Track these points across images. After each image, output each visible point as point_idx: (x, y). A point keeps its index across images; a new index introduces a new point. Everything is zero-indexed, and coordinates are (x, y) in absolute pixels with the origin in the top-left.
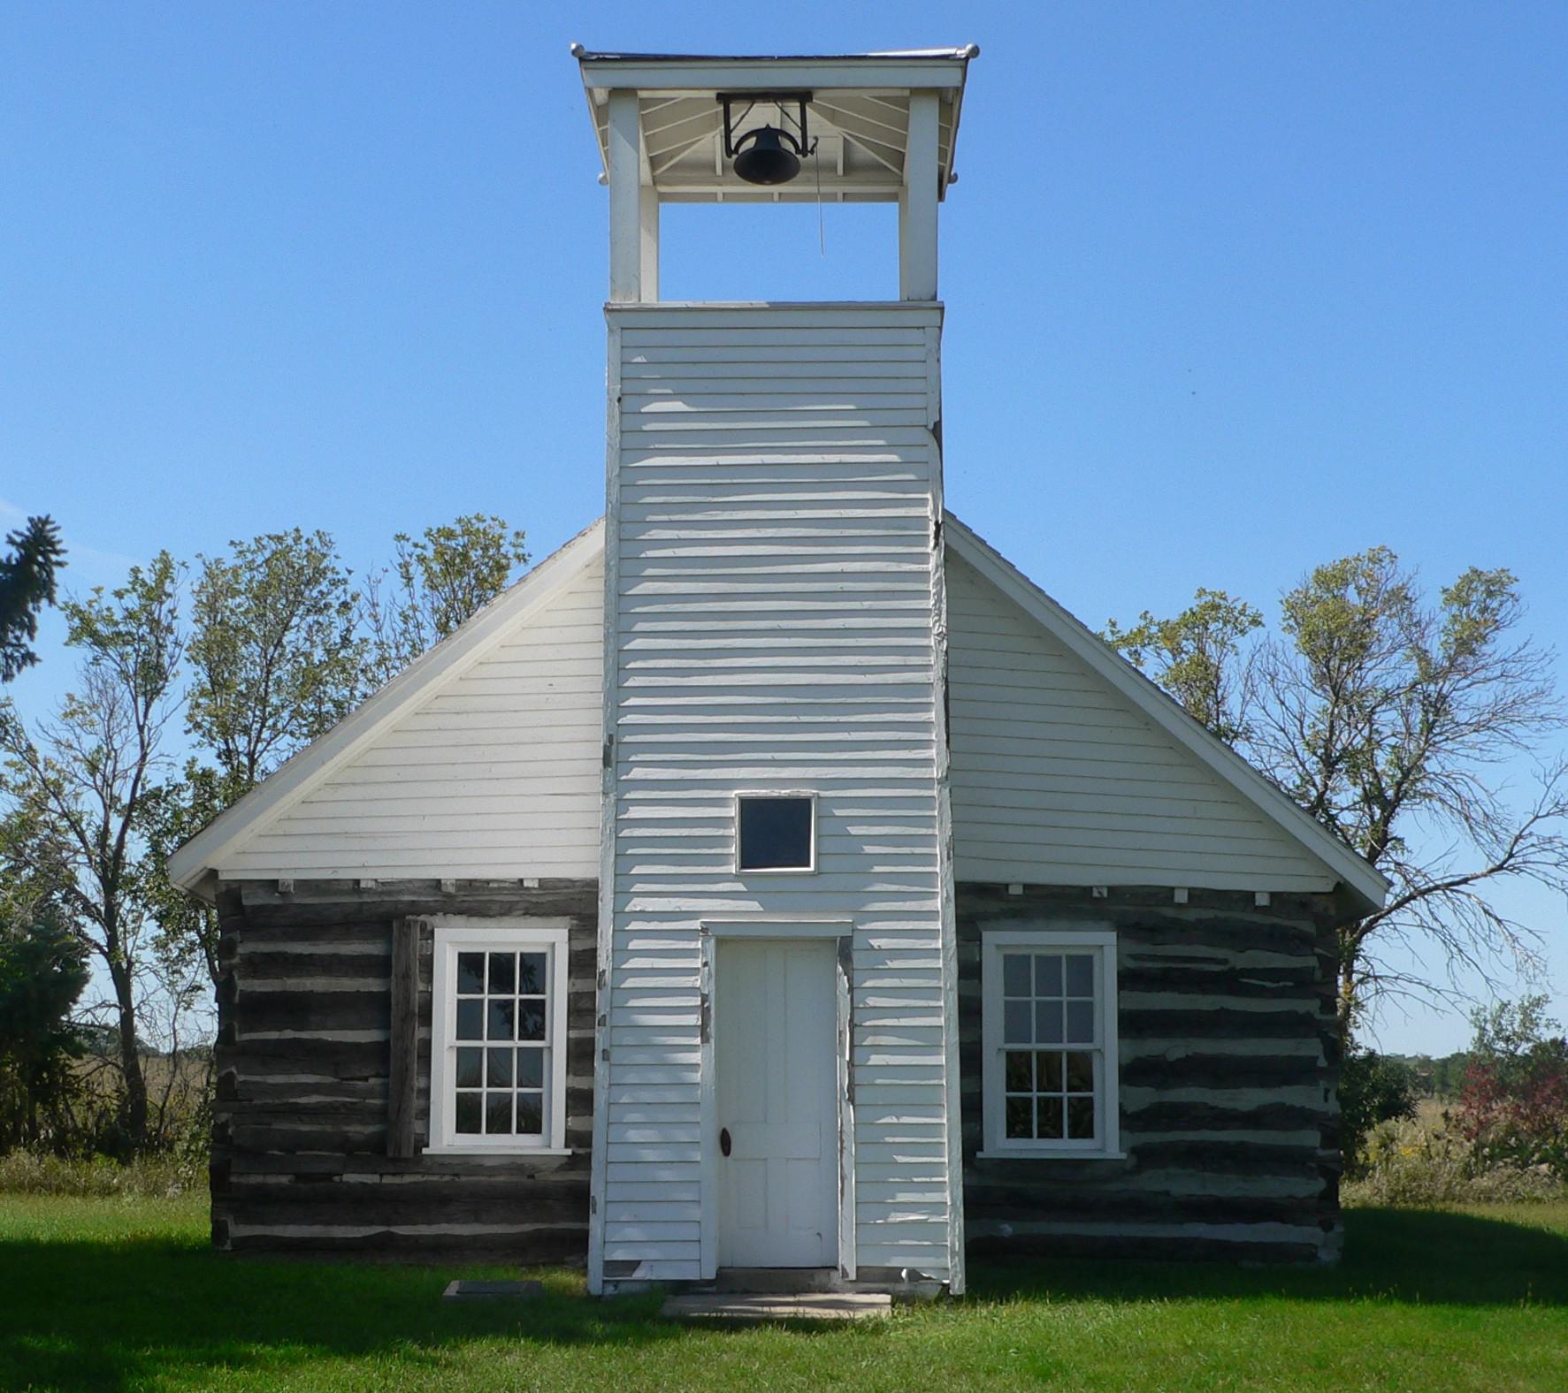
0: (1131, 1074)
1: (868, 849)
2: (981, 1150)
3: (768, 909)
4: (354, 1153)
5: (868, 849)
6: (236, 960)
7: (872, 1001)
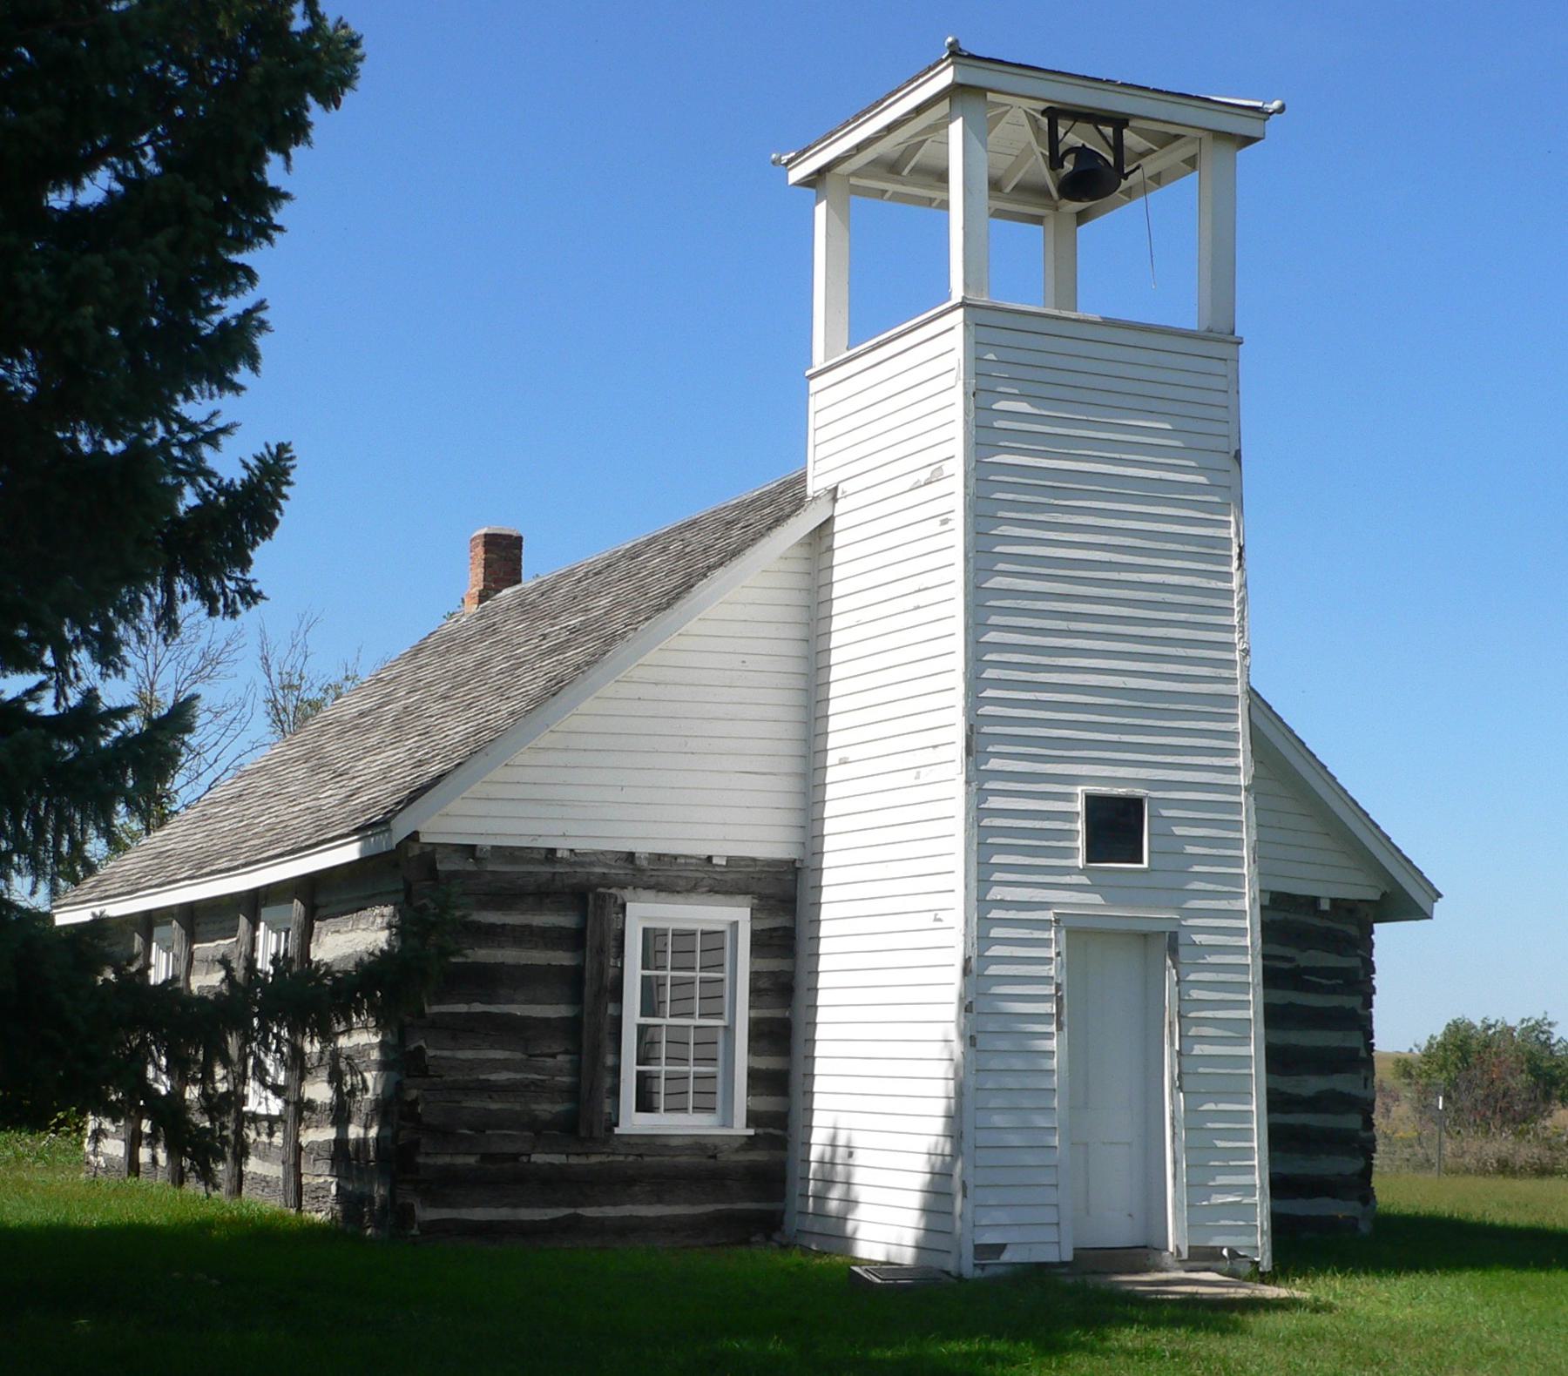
1: (1190, 849)
3: (1111, 902)
4: (540, 1131)
5: (1190, 849)
7: (1196, 994)
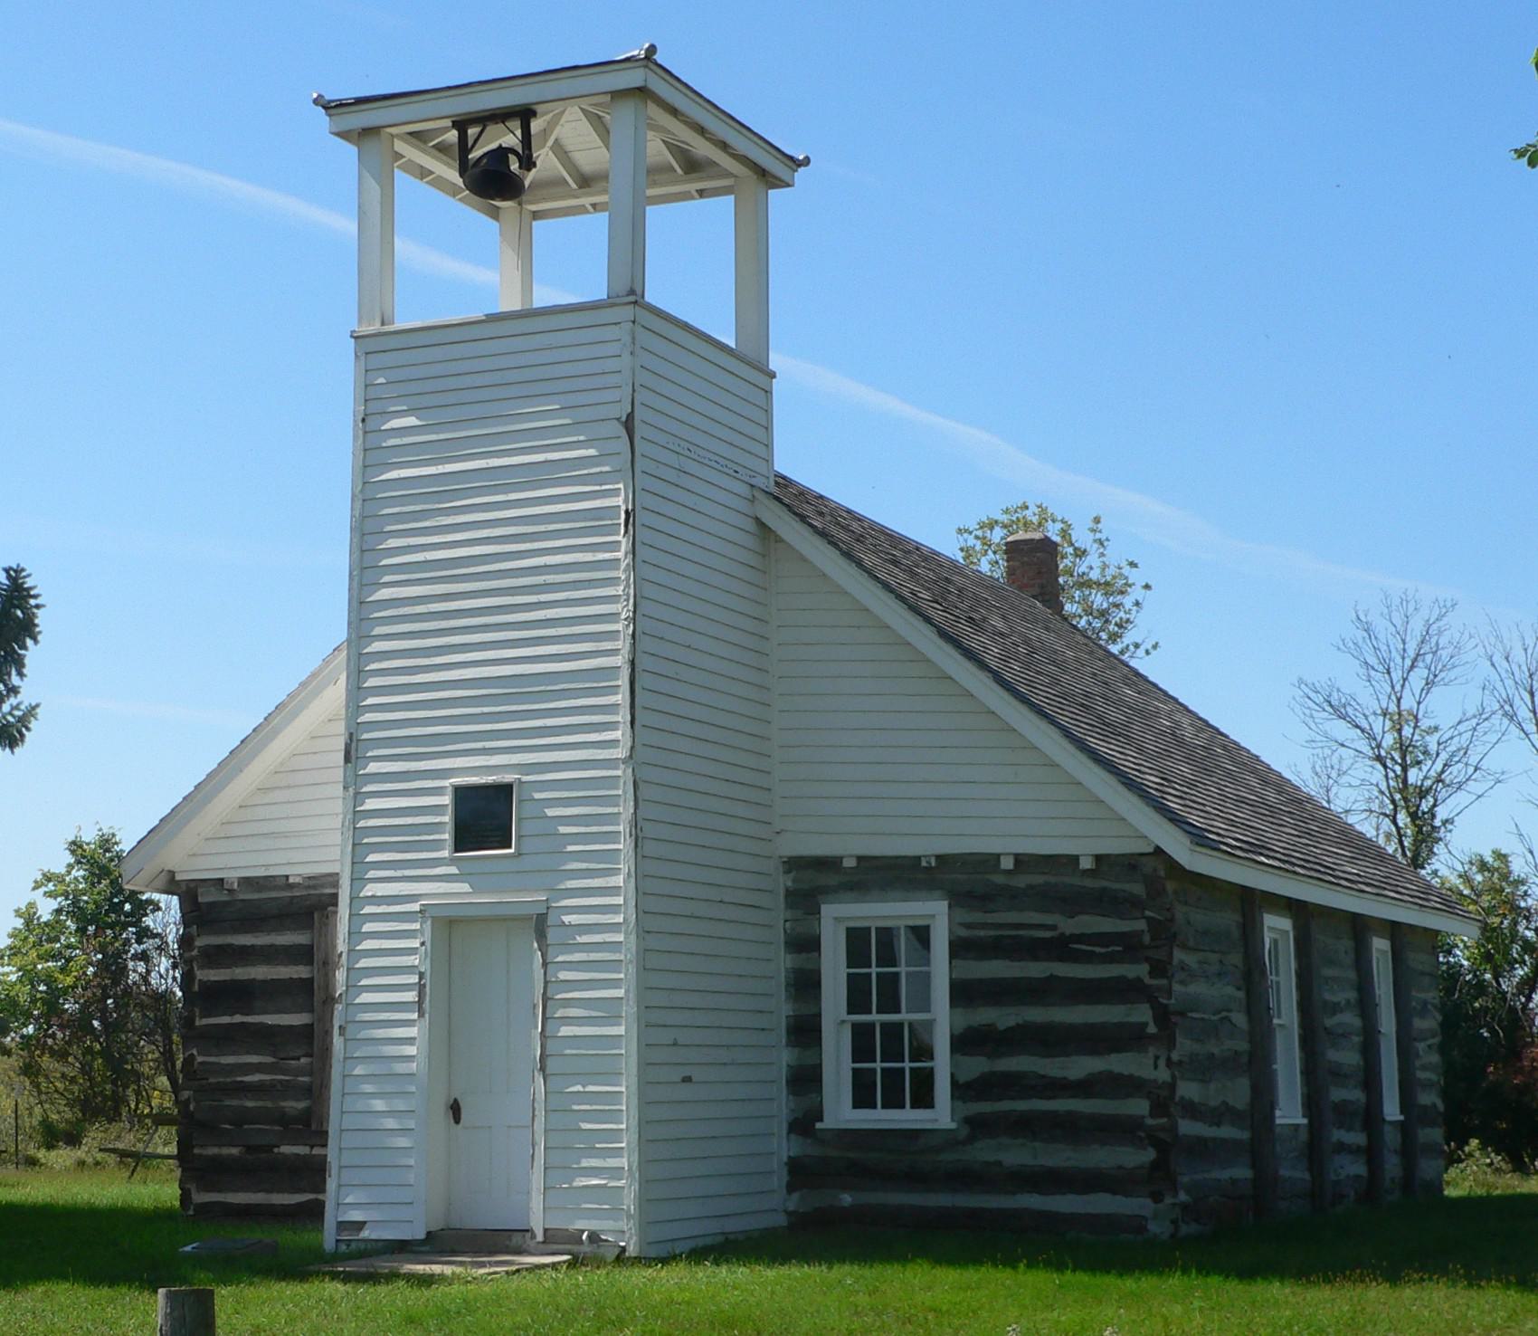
0: (963, 1043)
1: (563, 830)
2: (821, 1120)
3: (476, 890)
5: (563, 830)
6: (195, 953)
7: (563, 975)
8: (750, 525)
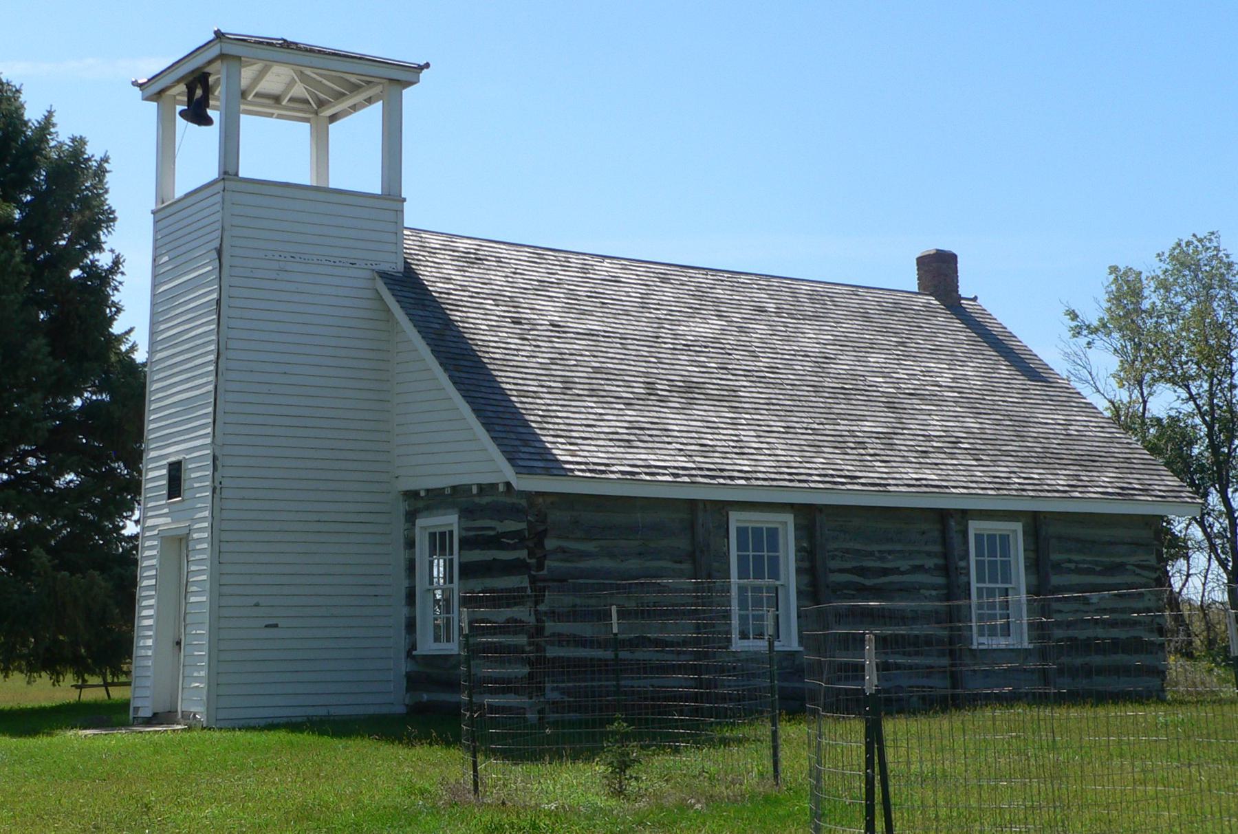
8: (369, 294)
